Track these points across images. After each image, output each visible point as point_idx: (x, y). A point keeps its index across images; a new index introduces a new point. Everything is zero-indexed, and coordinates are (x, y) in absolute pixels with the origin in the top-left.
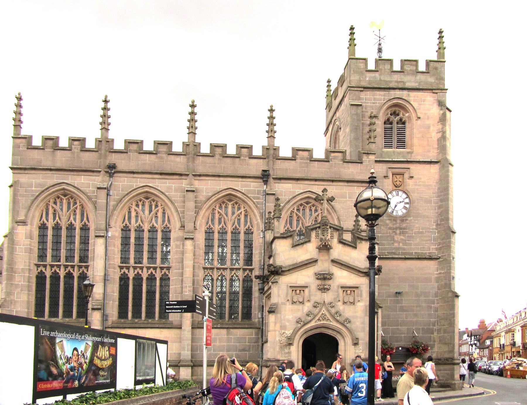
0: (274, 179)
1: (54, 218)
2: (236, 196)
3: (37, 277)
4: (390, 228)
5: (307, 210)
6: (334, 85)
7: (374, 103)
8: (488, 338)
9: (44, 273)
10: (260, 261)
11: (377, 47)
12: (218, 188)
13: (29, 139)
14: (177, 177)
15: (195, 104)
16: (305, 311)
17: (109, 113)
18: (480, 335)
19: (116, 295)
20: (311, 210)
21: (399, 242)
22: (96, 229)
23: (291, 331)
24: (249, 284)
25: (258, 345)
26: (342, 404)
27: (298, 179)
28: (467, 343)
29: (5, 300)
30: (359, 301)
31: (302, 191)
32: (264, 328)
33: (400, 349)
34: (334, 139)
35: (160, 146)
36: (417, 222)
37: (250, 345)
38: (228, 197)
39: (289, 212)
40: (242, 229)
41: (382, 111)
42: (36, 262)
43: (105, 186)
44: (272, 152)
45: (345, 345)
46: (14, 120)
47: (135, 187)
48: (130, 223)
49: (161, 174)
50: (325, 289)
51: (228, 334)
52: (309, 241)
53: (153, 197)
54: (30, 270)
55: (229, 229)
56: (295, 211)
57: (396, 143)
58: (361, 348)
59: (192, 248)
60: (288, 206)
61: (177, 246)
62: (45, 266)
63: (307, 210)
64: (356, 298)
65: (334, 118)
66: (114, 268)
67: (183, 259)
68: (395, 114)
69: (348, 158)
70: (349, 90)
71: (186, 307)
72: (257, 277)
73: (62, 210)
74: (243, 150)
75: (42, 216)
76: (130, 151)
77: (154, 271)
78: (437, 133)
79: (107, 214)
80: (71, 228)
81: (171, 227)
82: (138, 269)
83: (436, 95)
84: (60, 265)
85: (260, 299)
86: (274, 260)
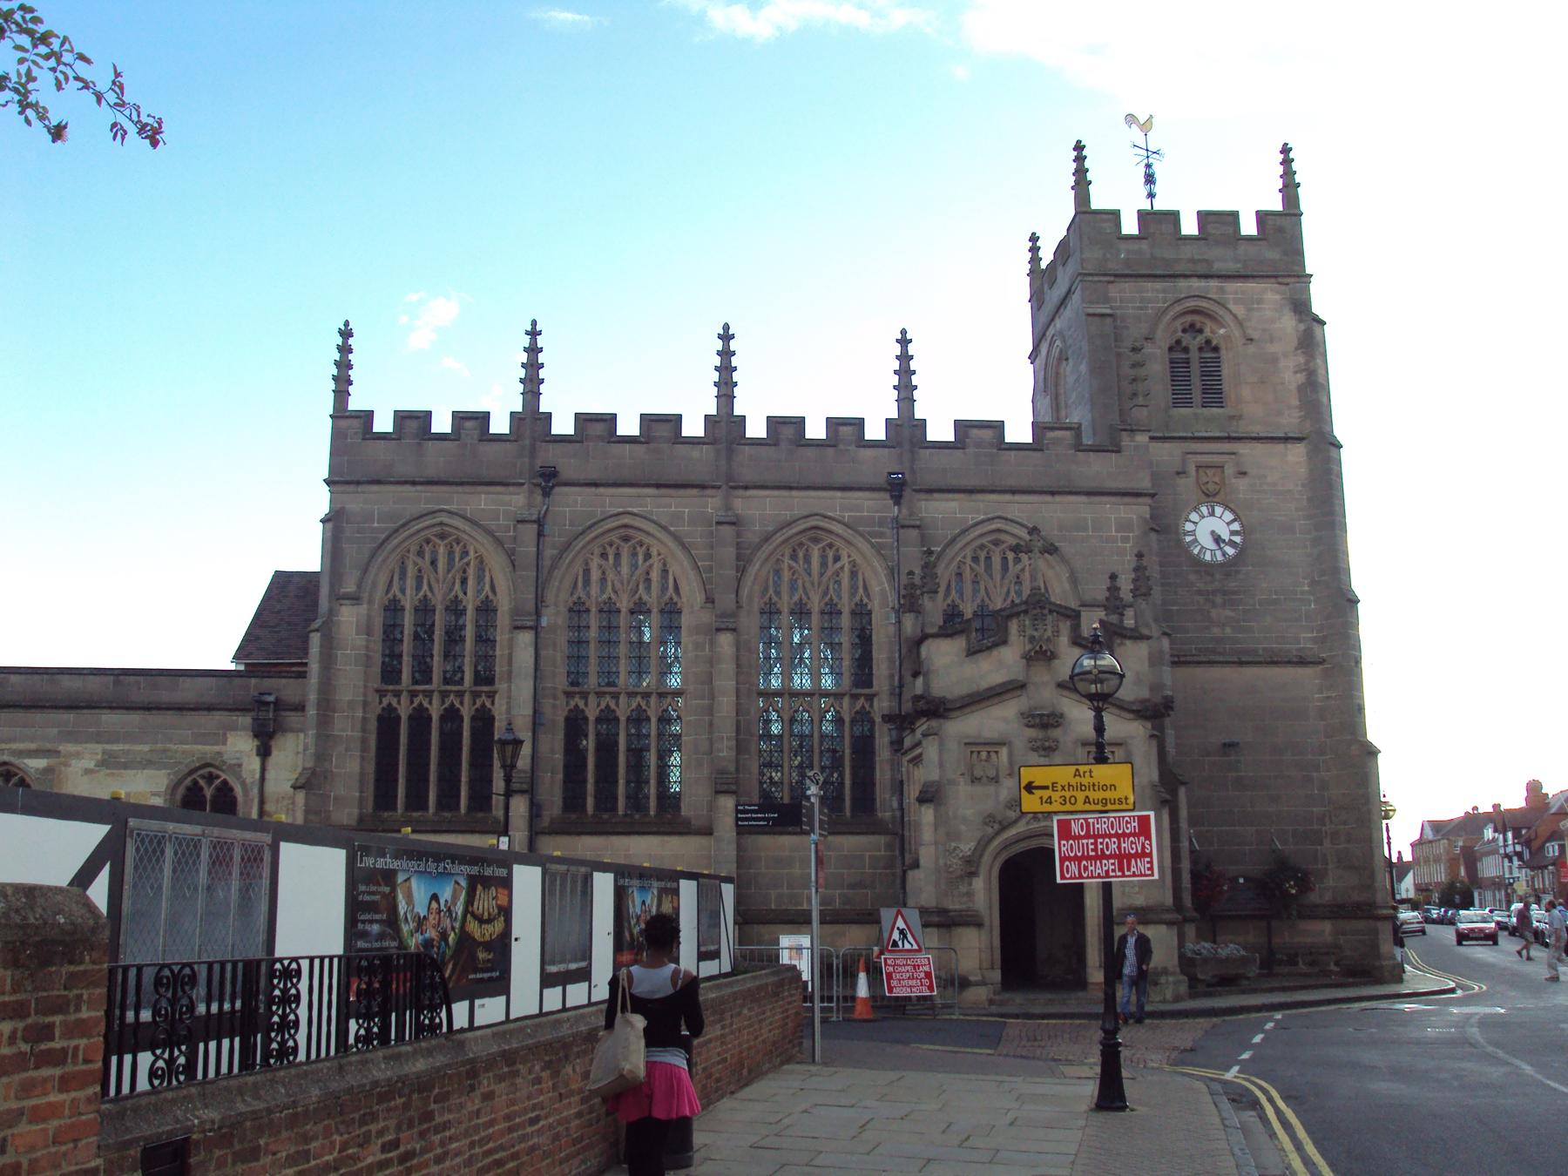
1: (419, 588)
2: (830, 532)
3: (380, 719)
4: (1199, 592)
6: (1047, 257)
7: (1141, 308)
8: (1549, 839)
10: (892, 676)
11: (1142, 170)
12: (788, 515)
14: (694, 492)
17: (541, 358)
20: (1006, 558)
21: (1223, 625)
23: (972, 845)
25: (894, 874)
26: (1332, 1175)
27: (971, 491)
28: (1496, 852)
29: (314, 773)
33: (1241, 880)
35: (654, 425)
38: (811, 534)
39: (955, 563)
47: (599, 517)
49: (658, 486)
52: (1005, 642)
53: (640, 536)
54: (365, 704)
56: (968, 560)
60: (950, 553)
61: (697, 646)
62: (397, 694)
63: (996, 561)
66: (555, 697)
68: (1192, 329)
69: (1087, 440)
72: (888, 718)
74: (469, 424)
75: (391, 582)
78: (1296, 372)
84: (433, 691)
85: (895, 766)
86: (926, 685)
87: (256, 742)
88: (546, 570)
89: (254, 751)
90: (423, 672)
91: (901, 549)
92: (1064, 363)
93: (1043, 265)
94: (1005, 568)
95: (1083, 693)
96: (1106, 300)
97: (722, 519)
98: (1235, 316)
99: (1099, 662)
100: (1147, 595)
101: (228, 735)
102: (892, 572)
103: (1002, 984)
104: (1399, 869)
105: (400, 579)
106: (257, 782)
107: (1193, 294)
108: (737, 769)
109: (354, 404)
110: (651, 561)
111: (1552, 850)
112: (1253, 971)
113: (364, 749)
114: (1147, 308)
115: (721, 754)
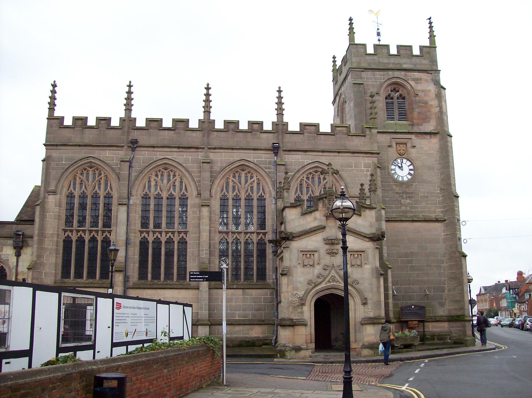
0: (283, 150)
3: (64, 241)
4: (397, 193)
5: (316, 179)
6: (339, 63)
8: (526, 292)
9: (71, 237)
10: (273, 225)
12: (232, 160)
13: (62, 119)
15: (132, 84)
16: (315, 273)
17: (133, 96)
18: (518, 288)
19: (137, 257)
21: (406, 206)
22: (119, 198)
23: (303, 292)
24: (263, 246)
29: (36, 263)
30: (366, 264)
31: (310, 161)
32: (278, 289)
33: (413, 307)
34: (340, 112)
36: (421, 187)
37: (265, 305)
38: (241, 168)
39: (299, 180)
40: (255, 196)
41: (383, 89)
42: (64, 227)
43: (128, 160)
44: (280, 127)
45: (355, 305)
46: (49, 103)
47: (155, 160)
48: (150, 192)
49: (179, 148)
50: (333, 253)
51: (243, 294)
52: (317, 210)
54: (58, 235)
55: (243, 196)
56: (305, 179)
57: (397, 116)
58: (370, 307)
59: (208, 214)
60: (297, 175)
61: (194, 212)
62: (71, 231)
63: (316, 179)
64: (363, 262)
65: (340, 92)
66: (135, 233)
67: (199, 224)
68: (395, 90)
69: (353, 131)
70: (351, 70)
71: (207, 277)
72: (270, 241)
73: (88, 180)
76: (151, 128)
77: (172, 235)
79: (129, 184)
80: (96, 196)
81: (188, 195)
82: (157, 234)
83: (430, 75)
85: (274, 261)
87: (15, 251)
88: (132, 181)
89: (14, 254)
90: (82, 222)
91: (277, 174)
92: (345, 103)
93: (337, 67)
94: (320, 182)
95: (337, 218)
96: (361, 78)
97: (204, 161)
98: (411, 86)
99: (344, 204)
100: (375, 191)
101: (4, 248)
102: (274, 183)
103: (315, 349)
104: (472, 302)
105: (74, 185)
106: (15, 267)
107: (395, 76)
108: (209, 263)
109: (57, 114)
110: (176, 178)
111: (527, 297)
112: (417, 342)
113: (57, 254)
114: (377, 82)
115: (203, 256)
